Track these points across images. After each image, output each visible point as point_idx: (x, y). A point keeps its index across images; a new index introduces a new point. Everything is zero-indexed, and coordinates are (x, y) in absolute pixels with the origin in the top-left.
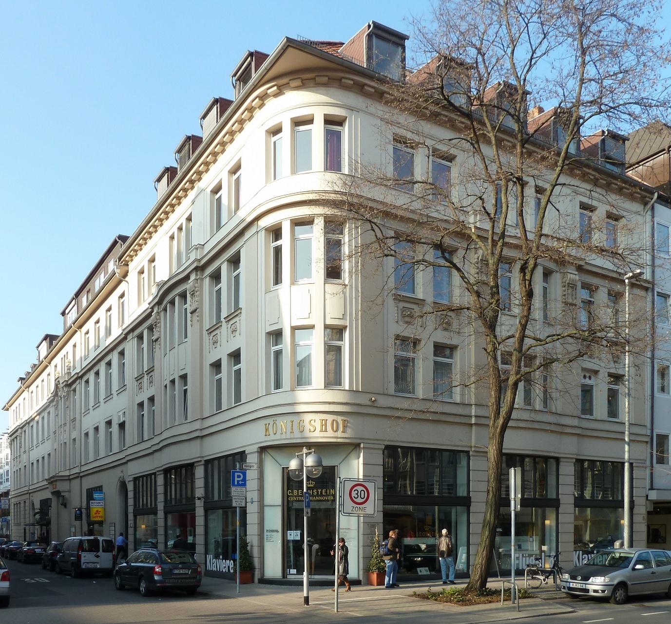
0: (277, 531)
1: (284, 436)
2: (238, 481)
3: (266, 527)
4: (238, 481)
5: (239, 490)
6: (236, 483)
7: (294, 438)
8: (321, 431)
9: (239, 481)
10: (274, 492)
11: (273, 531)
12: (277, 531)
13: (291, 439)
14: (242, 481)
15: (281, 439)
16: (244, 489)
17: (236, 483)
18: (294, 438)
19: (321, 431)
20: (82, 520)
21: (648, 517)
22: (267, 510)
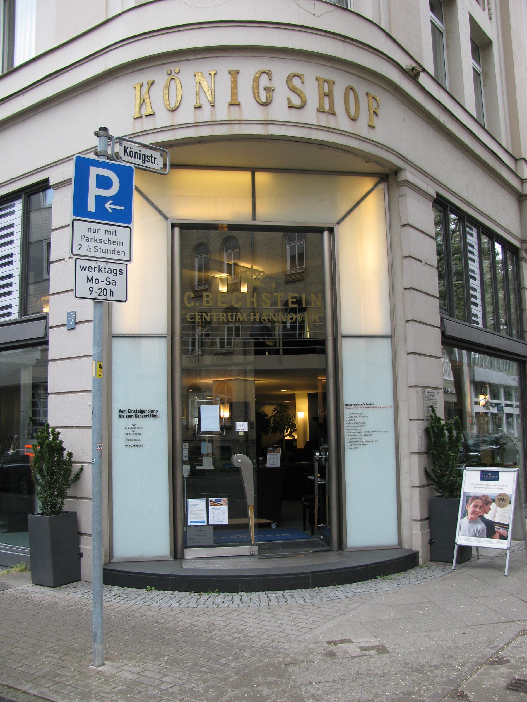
0: (153, 414)
1: (206, 115)
2: (100, 200)
3: (118, 405)
4: (100, 200)
5: (101, 235)
6: (91, 207)
7: (240, 122)
8: (320, 110)
9: (105, 199)
10: (146, 298)
11: (140, 414)
12: (153, 414)
13: (230, 122)
14: (116, 199)
15: (197, 125)
16: (122, 233)
17: (91, 207)
18: (240, 122)
19: (320, 110)
20: (499, 472)
21: (47, 378)
22: (120, 347)
